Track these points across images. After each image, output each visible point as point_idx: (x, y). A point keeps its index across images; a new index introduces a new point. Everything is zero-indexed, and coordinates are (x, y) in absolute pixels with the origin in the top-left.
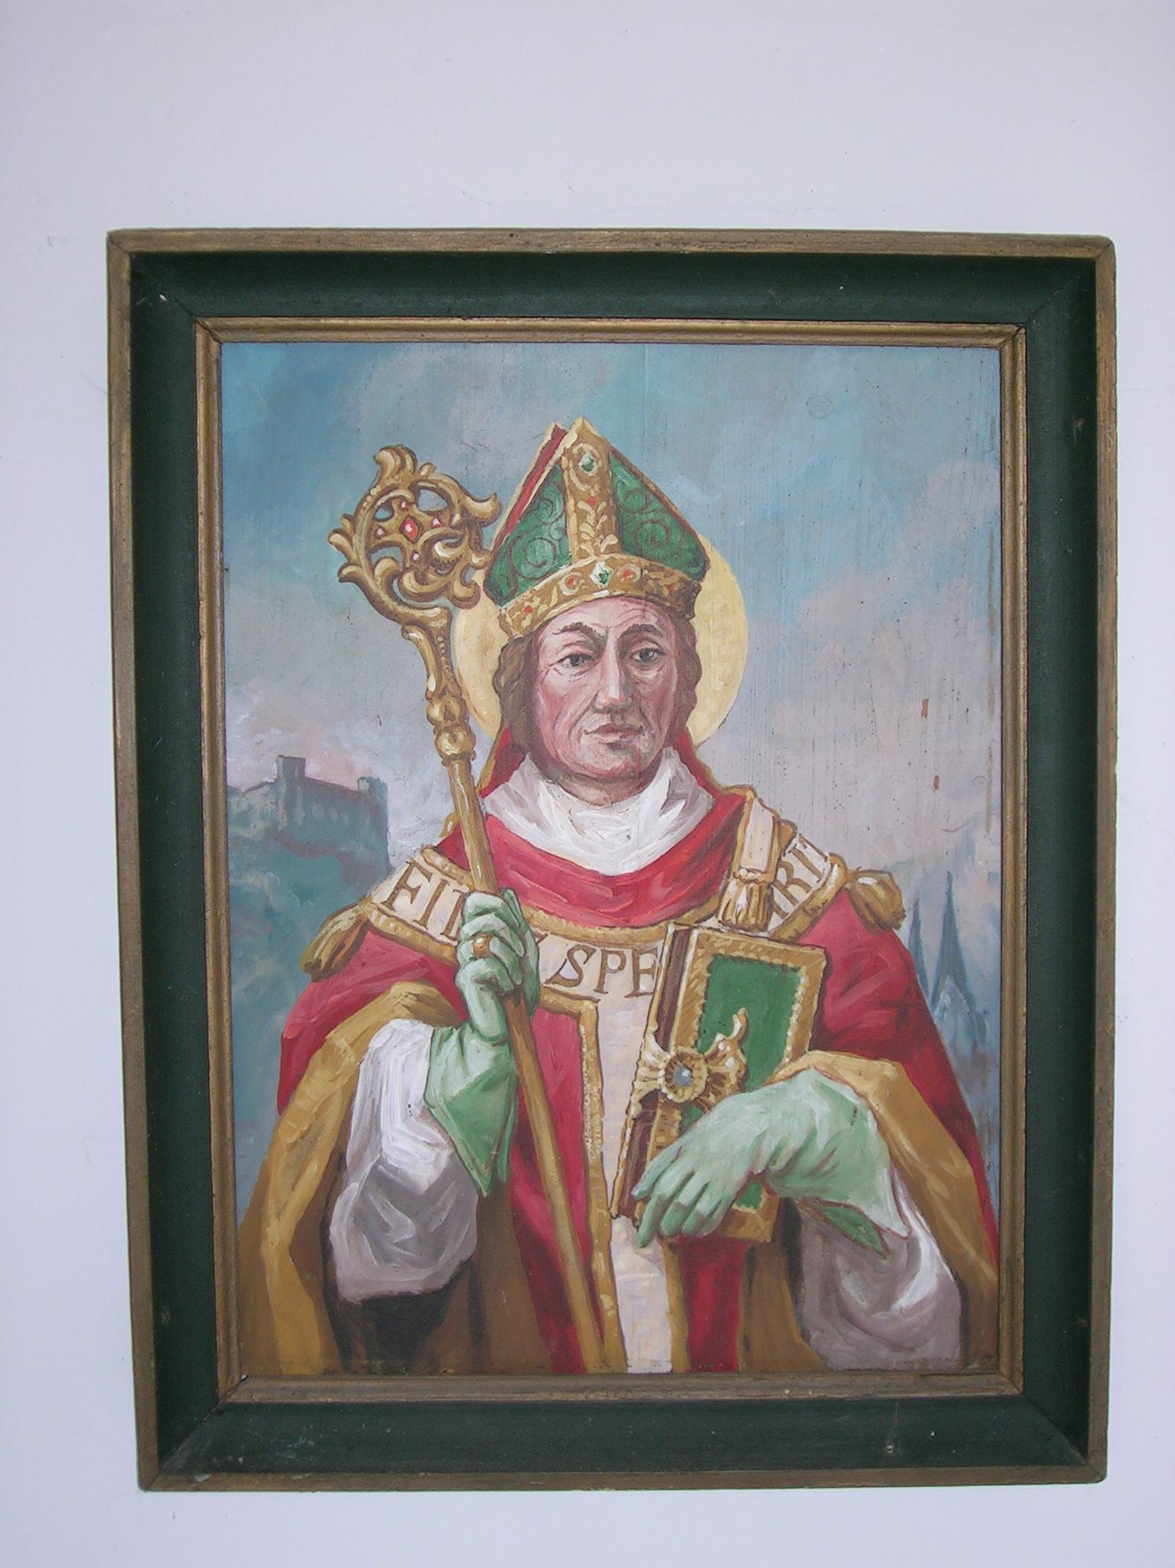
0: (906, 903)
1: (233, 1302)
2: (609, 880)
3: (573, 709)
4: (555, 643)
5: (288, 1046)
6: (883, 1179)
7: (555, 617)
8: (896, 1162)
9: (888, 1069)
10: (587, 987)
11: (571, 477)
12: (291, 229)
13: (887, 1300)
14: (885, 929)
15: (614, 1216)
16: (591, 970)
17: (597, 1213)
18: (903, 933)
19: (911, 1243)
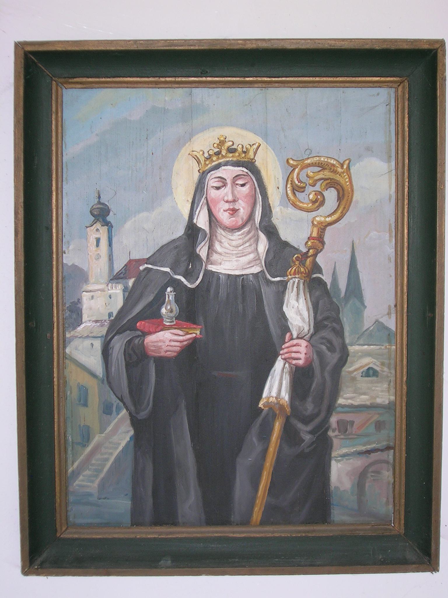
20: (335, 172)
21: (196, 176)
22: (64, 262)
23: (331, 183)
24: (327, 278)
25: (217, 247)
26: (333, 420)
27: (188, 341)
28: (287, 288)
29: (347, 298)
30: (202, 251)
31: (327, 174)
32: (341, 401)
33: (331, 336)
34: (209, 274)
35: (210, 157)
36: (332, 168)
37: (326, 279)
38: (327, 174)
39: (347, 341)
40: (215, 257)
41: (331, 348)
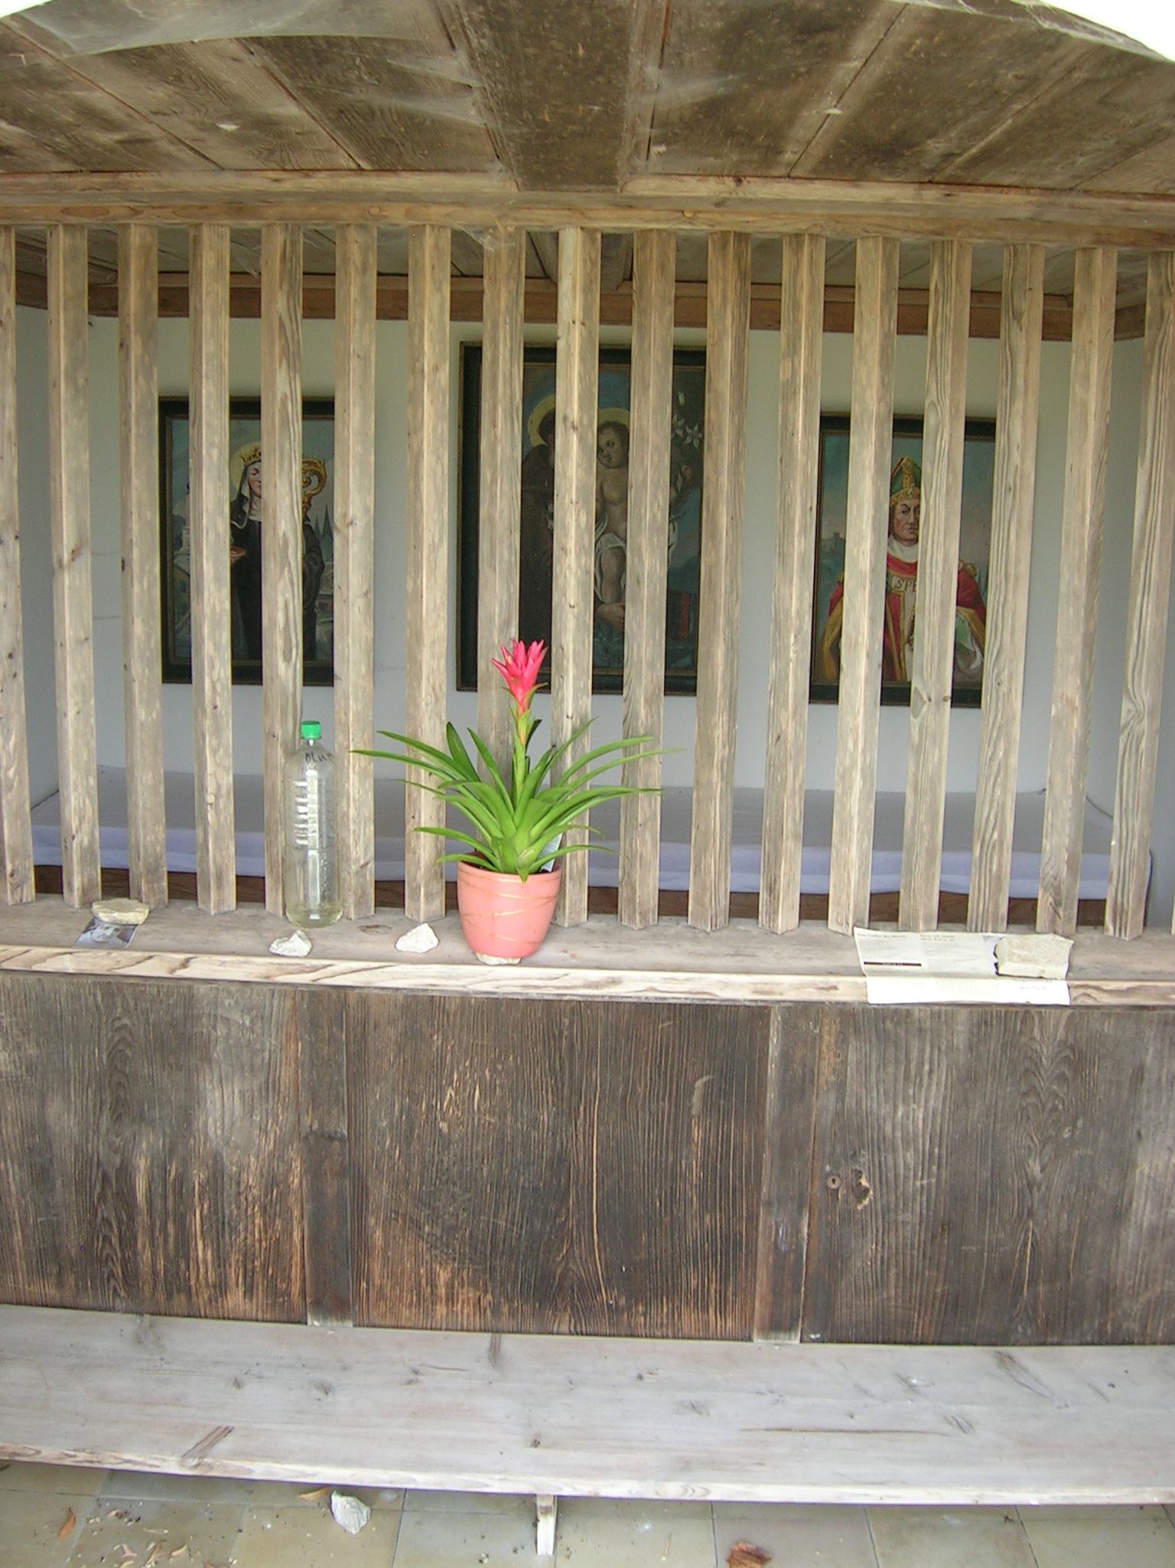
0: (977, 571)
1: (675, 1079)
2: (908, 564)
3: (903, 523)
4: (899, 508)
5: (832, 601)
6: (969, 639)
7: (767, 1430)
8: (973, 634)
9: (972, 611)
10: (903, 588)
11: (904, 470)
12: (462, 747)
13: (969, 666)
14: (972, 577)
15: (912, 536)
16: (904, 585)
17: (902, 642)
18: (977, 579)
19: (975, 653)
20: (316, 466)
21: (243, 468)
22: (175, 512)
23: (316, 473)
24: (313, 525)
25: (254, 506)
26: (317, 603)
27: (918, 236)
28: (20, 627)
29: (324, 536)
30: (246, 509)
31: (313, 467)
32: (321, 592)
33: (314, 556)
34: (249, 520)
35: (250, 458)
36: (315, 464)
37: (657, 1493)
38: (313, 467)
39: (324, 558)
40: (253, 512)
41: (315, 563)
